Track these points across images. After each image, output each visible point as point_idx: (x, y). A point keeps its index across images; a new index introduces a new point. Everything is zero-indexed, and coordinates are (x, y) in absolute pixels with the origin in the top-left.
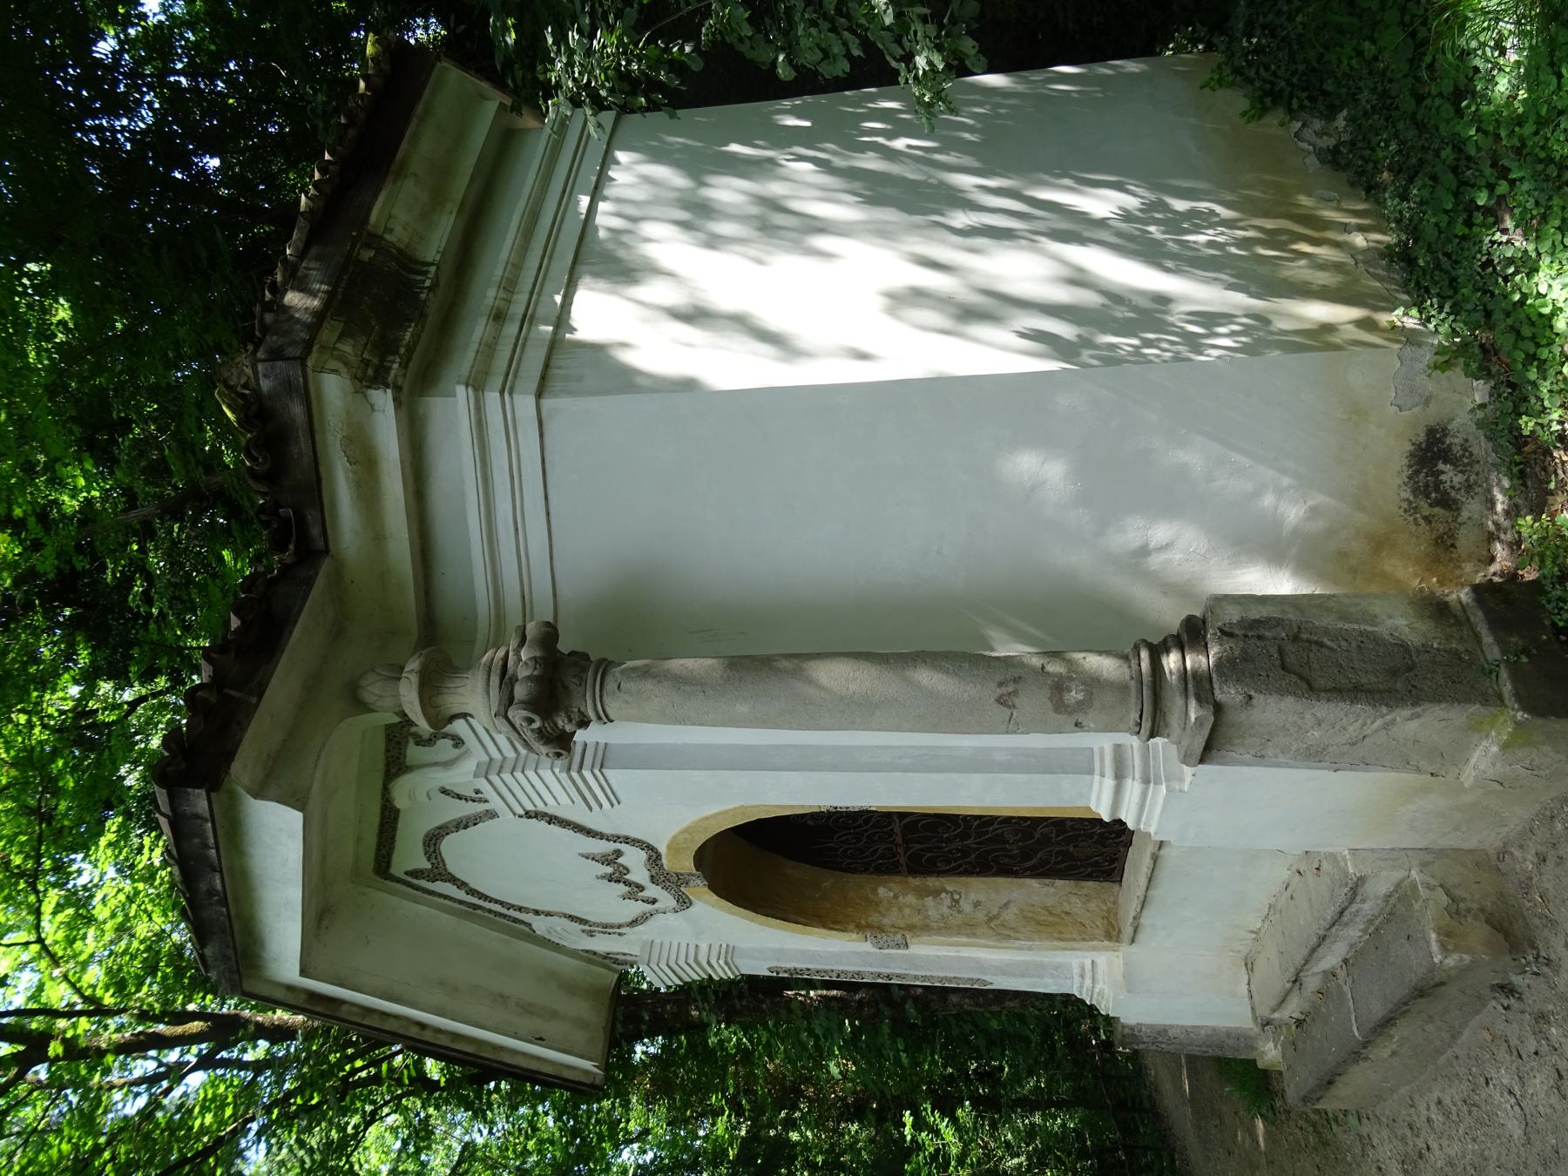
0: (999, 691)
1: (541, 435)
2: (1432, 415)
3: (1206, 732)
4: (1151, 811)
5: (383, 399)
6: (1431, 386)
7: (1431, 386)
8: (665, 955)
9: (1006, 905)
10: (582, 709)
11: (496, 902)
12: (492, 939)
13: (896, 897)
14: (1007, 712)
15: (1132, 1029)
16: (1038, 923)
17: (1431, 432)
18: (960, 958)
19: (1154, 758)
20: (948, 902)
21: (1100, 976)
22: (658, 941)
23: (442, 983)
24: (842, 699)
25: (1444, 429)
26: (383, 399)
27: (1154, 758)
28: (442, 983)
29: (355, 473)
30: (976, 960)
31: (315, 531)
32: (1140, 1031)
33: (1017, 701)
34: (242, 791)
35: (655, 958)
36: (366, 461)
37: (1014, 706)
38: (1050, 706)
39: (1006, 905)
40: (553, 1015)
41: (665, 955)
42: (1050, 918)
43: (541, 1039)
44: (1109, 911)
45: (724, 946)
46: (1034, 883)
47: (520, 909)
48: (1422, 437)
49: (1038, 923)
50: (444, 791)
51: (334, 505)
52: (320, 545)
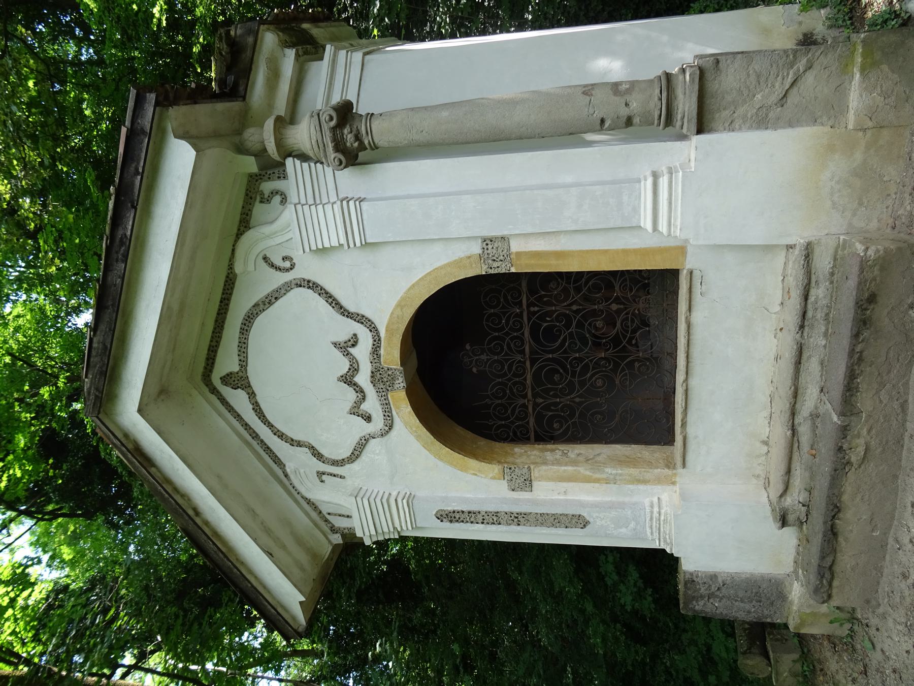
0: (584, 89)
1: (362, 69)
2: (805, 28)
3: (696, 87)
4: (676, 207)
5: (291, 53)
6: (800, 18)
7: (800, 18)
8: (368, 494)
9: (599, 455)
10: (359, 128)
11: (270, 426)
12: (256, 467)
13: (525, 452)
14: (588, 98)
15: (691, 574)
16: (619, 461)
17: (805, 35)
18: (567, 500)
19: (675, 191)
20: (560, 453)
21: (664, 503)
22: (364, 488)
23: (219, 477)
24: (499, 102)
25: (812, 34)
26: (291, 53)
27: (675, 191)
28: (219, 477)
29: (268, 74)
30: (579, 501)
31: (241, 88)
32: (697, 577)
33: (593, 92)
34: (170, 129)
35: (361, 494)
36: (275, 75)
37: (592, 95)
38: (611, 92)
39: (599, 455)
40: (284, 547)
41: (368, 494)
42: (628, 460)
43: (271, 554)
44: (668, 457)
45: (408, 493)
46: (618, 446)
47: (281, 436)
48: (801, 37)
49: (619, 461)
50: (265, 259)
51: (254, 83)
52: (242, 93)
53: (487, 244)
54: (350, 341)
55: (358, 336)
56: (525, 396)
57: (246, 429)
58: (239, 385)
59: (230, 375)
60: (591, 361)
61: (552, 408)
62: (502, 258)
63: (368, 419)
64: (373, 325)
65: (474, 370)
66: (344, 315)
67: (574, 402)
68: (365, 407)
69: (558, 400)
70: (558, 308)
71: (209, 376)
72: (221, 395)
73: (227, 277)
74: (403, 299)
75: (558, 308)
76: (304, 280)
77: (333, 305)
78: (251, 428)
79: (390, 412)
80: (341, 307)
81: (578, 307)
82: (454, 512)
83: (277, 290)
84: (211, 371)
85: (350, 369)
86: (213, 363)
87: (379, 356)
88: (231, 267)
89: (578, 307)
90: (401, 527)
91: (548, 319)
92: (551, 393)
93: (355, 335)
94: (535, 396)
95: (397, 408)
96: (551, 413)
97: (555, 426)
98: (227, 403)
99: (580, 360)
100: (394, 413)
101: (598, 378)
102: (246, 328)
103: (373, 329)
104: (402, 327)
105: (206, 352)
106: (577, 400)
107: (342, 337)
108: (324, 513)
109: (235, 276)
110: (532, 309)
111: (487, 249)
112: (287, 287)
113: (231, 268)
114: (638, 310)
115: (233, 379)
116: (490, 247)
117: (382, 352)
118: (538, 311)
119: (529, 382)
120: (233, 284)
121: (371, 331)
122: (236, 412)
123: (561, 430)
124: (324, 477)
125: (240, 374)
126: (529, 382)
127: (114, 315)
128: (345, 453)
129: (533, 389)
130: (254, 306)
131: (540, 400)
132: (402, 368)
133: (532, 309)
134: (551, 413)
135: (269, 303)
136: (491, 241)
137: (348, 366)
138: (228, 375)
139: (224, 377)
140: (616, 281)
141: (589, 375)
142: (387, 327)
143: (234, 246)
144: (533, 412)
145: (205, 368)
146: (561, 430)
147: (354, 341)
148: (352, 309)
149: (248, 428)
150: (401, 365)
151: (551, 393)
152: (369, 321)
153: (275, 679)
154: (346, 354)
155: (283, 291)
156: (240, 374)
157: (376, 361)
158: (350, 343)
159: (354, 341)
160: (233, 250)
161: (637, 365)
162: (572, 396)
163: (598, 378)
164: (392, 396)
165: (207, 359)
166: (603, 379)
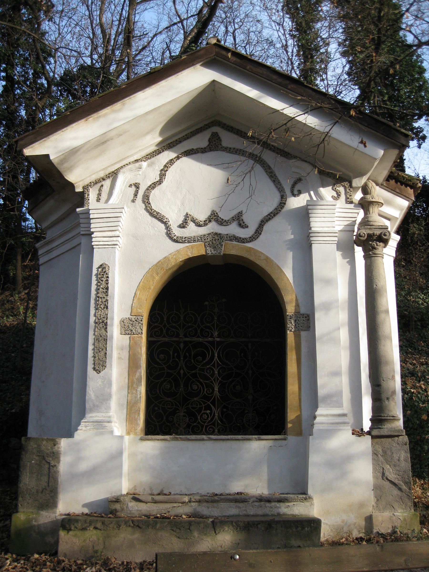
53: (306, 317)
54: (244, 223)
55: (246, 229)
56: (185, 336)
57: (176, 140)
58: (211, 144)
59: (219, 139)
60: (212, 382)
61: (176, 354)
62: (297, 326)
63: (183, 226)
64: (254, 239)
65: (206, 303)
66: (262, 222)
67: (180, 369)
68: (192, 225)
69: (182, 359)
70: (182, 361)
71: (219, 125)
72: (204, 130)
73: (289, 154)
74: (272, 261)
75: (182, 361)
76: (285, 201)
77: (269, 217)
78: (177, 144)
79: (189, 242)
80: (267, 221)
81: (182, 374)
82: (108, 277)
83: (279, 183)
84: (223, 127)
85: (223, 219)
86: (229, 130)
87: (231, 240)
88: (295, 157)
89: (182, 374)
90: (96, 237)
91: (242, 354)
92: (187, 354)
93: (247, 227)
94: (186, 343)
95: (192, 247)
96: (171, 353)
97: (161, 355)
98: (198, 133)
99: (213, 375)
100: (187, 245)
101: (198, 386)
102: (254, 157)
103: (253, 239)
104: (252, 258)
105: (237, 128)
106: (182, 372)
107: (246, 218)
108: (103, 183)
109: (290, 159)
110: (250, 344)
111: (303, 317)
112: (281, 190)
113: (295, 157)
114: (247, 413)
115: (217, 141)
116: (304, 319)
117: (234, 243)
118: (180, 348)
119: (195, 339)
120: (284, 156)
121: (250, 238)
122: (191, 137)
123: (158, 360)
124: (134, 188)
125: (220, 147)
126: (195, 339)
127: (264, 77)
128: (154, 206)
129: (191, 342)
130: (269, 166)
131: (182, 346)
132: (222, 254)
133: (250, 344)
134: (171, 353)
135: (271, 176)
136: (308, 320)
137: (225, 218)
138: (219, 138)
139: (218, 135)
140: (201, 398)
141: (201, 380)
142: (253, 248)
143: (309, 162)
144: (171, 341)
145: (225, 124)
146: (158, 360)
147: (242, 225)
148: (265, 228)
149: (177, 142)
150: (224, 254)
151: (187, 354)
152: (257, 238)
153: (343, 71)
154: (234, 219)
155: (279, 186)
156: (220, 147)
157: (228, 238)
158: (241, 222)
159: (242, 225)
160: (306, 161)
161: (208, 412)
162: (185, 368)
163: (198, 386)
164: (201, 245)
165: (232, 127)
166: (197, 389)
